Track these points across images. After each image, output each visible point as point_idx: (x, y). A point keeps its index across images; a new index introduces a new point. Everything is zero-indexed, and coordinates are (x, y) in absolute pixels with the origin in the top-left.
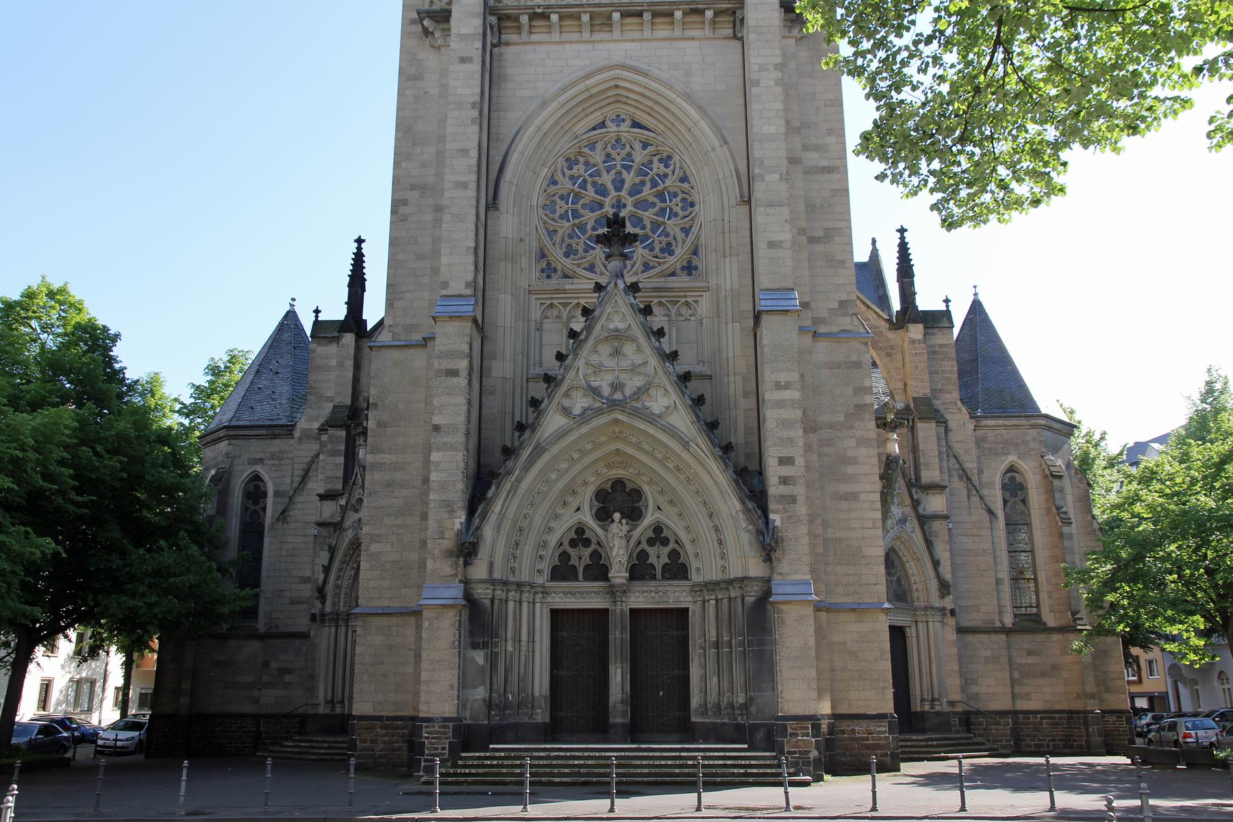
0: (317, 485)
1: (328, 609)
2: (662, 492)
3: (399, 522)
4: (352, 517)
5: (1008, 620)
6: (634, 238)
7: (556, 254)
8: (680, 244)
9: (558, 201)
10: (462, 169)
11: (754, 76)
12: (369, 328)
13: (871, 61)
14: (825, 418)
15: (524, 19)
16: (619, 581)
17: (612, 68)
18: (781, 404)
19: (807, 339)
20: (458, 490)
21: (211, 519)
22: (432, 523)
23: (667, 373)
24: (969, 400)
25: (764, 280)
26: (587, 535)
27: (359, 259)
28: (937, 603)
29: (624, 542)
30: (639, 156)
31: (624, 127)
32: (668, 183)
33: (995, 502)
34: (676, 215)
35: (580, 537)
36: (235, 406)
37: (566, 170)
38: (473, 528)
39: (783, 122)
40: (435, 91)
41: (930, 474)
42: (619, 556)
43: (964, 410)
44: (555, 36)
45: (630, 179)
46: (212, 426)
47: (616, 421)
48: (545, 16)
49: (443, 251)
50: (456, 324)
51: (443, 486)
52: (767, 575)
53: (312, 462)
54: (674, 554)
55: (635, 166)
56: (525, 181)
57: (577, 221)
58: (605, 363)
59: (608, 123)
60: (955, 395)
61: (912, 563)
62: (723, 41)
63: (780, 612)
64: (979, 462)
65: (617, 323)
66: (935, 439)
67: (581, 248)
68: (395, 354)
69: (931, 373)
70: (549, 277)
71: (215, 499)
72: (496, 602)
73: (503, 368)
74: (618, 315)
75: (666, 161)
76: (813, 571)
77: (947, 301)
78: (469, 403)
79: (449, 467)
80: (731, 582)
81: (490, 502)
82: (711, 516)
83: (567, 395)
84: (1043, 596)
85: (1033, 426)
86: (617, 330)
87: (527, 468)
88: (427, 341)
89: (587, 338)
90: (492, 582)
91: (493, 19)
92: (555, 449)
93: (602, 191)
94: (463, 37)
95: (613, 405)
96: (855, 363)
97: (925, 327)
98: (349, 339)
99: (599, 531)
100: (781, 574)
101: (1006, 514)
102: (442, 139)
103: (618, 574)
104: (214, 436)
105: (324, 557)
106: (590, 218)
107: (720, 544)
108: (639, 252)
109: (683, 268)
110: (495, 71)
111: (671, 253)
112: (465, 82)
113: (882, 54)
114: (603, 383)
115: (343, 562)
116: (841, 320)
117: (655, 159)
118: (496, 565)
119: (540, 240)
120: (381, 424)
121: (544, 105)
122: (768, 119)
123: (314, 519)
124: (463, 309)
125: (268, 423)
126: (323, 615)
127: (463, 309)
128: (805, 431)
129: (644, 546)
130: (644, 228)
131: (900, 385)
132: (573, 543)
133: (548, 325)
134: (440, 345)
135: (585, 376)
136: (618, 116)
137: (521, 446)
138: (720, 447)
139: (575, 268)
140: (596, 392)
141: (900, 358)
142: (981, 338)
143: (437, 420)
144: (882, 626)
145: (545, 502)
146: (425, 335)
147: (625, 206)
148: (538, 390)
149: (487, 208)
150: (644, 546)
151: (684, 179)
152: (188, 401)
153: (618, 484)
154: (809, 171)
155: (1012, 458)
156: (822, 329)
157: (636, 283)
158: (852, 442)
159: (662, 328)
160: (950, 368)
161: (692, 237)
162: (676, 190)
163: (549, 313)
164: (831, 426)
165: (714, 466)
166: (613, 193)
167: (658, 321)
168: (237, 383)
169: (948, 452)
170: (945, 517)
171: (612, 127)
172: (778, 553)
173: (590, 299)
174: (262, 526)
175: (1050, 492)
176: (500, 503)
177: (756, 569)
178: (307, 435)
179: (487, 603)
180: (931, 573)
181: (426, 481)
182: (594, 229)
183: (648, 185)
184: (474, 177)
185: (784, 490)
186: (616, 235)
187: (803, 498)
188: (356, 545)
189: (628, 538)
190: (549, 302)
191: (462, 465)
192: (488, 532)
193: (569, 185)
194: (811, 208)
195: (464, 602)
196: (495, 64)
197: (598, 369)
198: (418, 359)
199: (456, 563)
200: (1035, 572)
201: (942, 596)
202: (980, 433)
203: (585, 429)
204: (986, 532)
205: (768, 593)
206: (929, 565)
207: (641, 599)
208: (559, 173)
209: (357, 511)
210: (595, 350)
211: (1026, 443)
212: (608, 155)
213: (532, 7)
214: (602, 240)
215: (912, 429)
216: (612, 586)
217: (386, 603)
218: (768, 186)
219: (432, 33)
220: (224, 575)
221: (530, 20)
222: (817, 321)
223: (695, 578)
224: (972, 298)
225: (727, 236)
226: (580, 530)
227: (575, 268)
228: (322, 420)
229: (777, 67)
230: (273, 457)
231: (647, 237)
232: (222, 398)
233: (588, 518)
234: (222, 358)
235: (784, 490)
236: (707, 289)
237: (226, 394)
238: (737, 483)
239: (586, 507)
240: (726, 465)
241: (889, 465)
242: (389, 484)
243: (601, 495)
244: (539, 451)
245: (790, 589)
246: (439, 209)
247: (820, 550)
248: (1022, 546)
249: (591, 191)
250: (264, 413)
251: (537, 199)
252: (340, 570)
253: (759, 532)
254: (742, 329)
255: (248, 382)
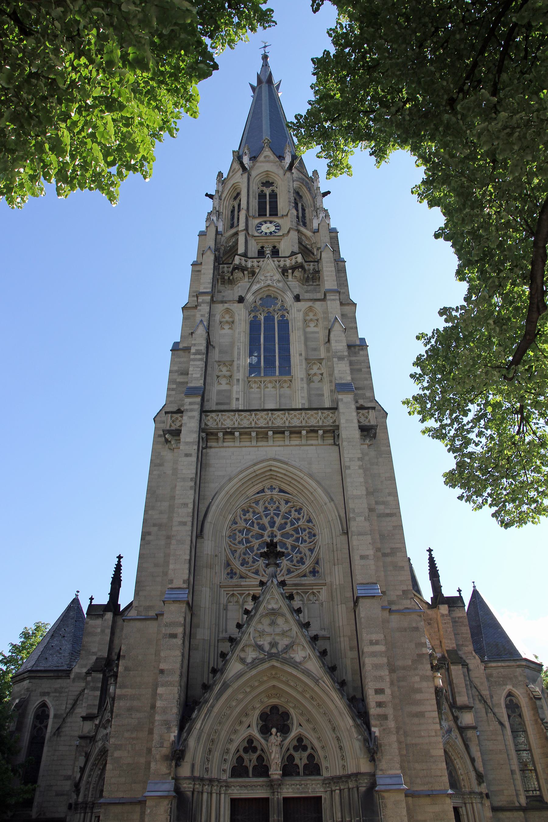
0: (81, 711)
1: (80, 800)
2: (302, 714)
3: (134, 735)
4: (102, 732)
5: (523, 801)
6: (282, 554)
7: (236, 564)
8: (308, 558)
9: (238, 533)
10: (184, 514)
11: (347, 464)
12: (122, 608)
13: (450, 430)
14: (399, 663)
15: (221, 435)
16: (276, 777)
17: (270, 459)
18: (374, 654)
19: (386, 614)
20: (173, 713)
21: (12, 733)
22: (156, 737)
23: (304, 636)
24: (479, 651)
25: (359, 578)
26: (255, 744)
27: (118, 568)
28: (477, 789)
29: (278, 749)
30: (284, 508)
31: (275, 492)
32: (300, 523)
33: (503, 717)
34: (305, 541)
35: (250, 745)
36: (36, 657)
37: (242, 516)
38: (182, 740)
39: (364, 488)
40: (169, 472)
41: (462, 699)
42: (275, 759)
43: (477, 657)
44: (237, 444)
45: (278, 521)
46: (20, 670)
47: (273, 667)
48: (232, 433)
49: (171, 561)
50: (177, 605)
51: (164, 711)
52: (372, 771)
53: (80, 694)
54: (311, 757)
55: (281, 513)
56: (218, 522)
57: (248, 545)
58: (266, 630)
59: (266, 490)
60: (471, 648)
61: (458, 760)
62: (329, 447)
63: (383, 798)
64: (490, 690)
65: (273, 605)
66: (462, 676)
67: (250, 560)
68: (138, 624)
69: (455, 634)
70: (232, 578)
71: (16, 720)
72: (196, 793)
73: (203, 634)
74: (274, 600)
75: (299, 511)
76: (402, 768)
77: (459, 591)
78: (183, 655)
79: (169, 697)
80: (349, 776)
81: (194, 721)
82: (334, 730)
83: (243, 650)
84: (542, 782)
85: (519, 666)
86: (273, 609)
87: (217, 698)
88: (159, 615)
89: (255, 614)
90: (193, 778)
91: (204, 435)
92: (236, 686)
93: (263, 528)
94: (187, 443)
95: (271, 656)
96: (414, 628)
97: (449, 607)
98: (109, 616)
99: (263, 741)
100: (381, 770)
101: (510, 724)
102: (173, 498)
103: (275, 772)
104: (21, 677)
105: (81, 761)
106: (256, 543)
107: (341, 752)
108: (285, 563)
109: (310, 572)
110: (204, 462)
111: (303, 563)
112: (188, 467)
113: (456, 426)
114: (265, 643)
115: (94, 765)
116: (405, 602)
117: (293, 510)
118: (196, 767)
119: (227, 556)
120: (127, 669)
121: (230, 480)
122: (356, 486)
123: (77, 734)
124: (181, 596)
125: (55, 668)
126: (77, 804)
127: (181, 596)
128: (390, 672)
129: (292, 751)
130: (287, 549)
131: (437, 642)
132: (246, 750)
133: (231, 607)
134: (166, 618)
135: (254, 638)
136: (271, 486)
137: (214, 684)
138: (338, 683)
139: (247, 572)
140: (260, 648)
141: (436, 625)
142: (481, 613)
143: (162, 666)
144: (448, 805)
145: (227, 723)
146: (157, 612)
147: (276, 536)
148: (225, 647)
149: (197, 537)
150: (292, 751)
151: (309, 521)
152: (7, 654)
153: (274, 708)
154: (380, 516)
155: (509, 687)
156: (394, 608)
157: (284, 581)
158: (417, 679)
159: (300, 608)
160: (466, 630)
161: (315, 554)
162: (305, 527)
163: (232, 600)
164: (404, 668)
165: (335, 696)
166: (269, 529)
167: (297, 604)
168: (38, 643)
169: (471, 685)
170: (474, 728)
171: (268, 492)
172: (379, 754)
173: (258, 591)
174: (44, 738)
175: (536, 709)
176: (200, 722)
177: (365, 767)
178: (79, 677)
179: (189, 794)
180: (471, 768)
181: (153, 707)
182: (258, 549)
183: (289, 524)
184: (190, 519)
185: (379, 711)
186: (272, 552)
187: (392, 716)
188: (104, 752)
189: (281, 745)
190: (231, 593)
191: (177, 696)
192: (192, 742)
193: (244, 524)
194: (382, 537)
195: (174, 794)
196: (204, 458)
197: (262, 634)
198: (152, 626)
199: (170, 765)
200: (534, 765)
201: (479, 784)
202: (488, 671)
203: (254, 672)
204: (500, 738)
205: (374, 784)
206: (469, 762)
207: (290, 790)
208: (238, 517)
209: (105, 728)
210: (260, 622)
211: (516, 677)
212: (266, 508)
213: (225, 429)
214: (264, 555)
215: (448, 670)
216: (272, 781)
217: (121, 795)
218: (358, 523)
219: (170, 442)
220: (15, 774)
221: (224, 435)
222: (391, 603)
223: (325, 774)
224: (472, 589)
225: (335, 553)
226: (250, 740)
227: (247, 572)
228: (89, 667)
229: (359, 459)
230: (56, 691)
231: (289, 554)
232: (28, 653)
233: (256, 733)
234: (31, 627)
235: (379, 711)
236: (325, 585)
237: (31, 650)
238: (349, 706)
239: (254, 725)
240: (343, 695)
241: (438, 691)
242: (130, 709)
243: (263, 716)
244: (226, 686)
245: (388, 781)
246: (169, 537)
247: (404, 752)
248: (523, 747)
249: (256, 528)
250: (53, 662)
251: (225, 532)
252: (91, 770)
253: (366, 741)
254: (347, 608)
255: (46, 642)
